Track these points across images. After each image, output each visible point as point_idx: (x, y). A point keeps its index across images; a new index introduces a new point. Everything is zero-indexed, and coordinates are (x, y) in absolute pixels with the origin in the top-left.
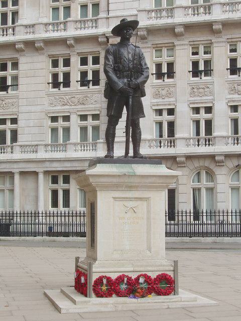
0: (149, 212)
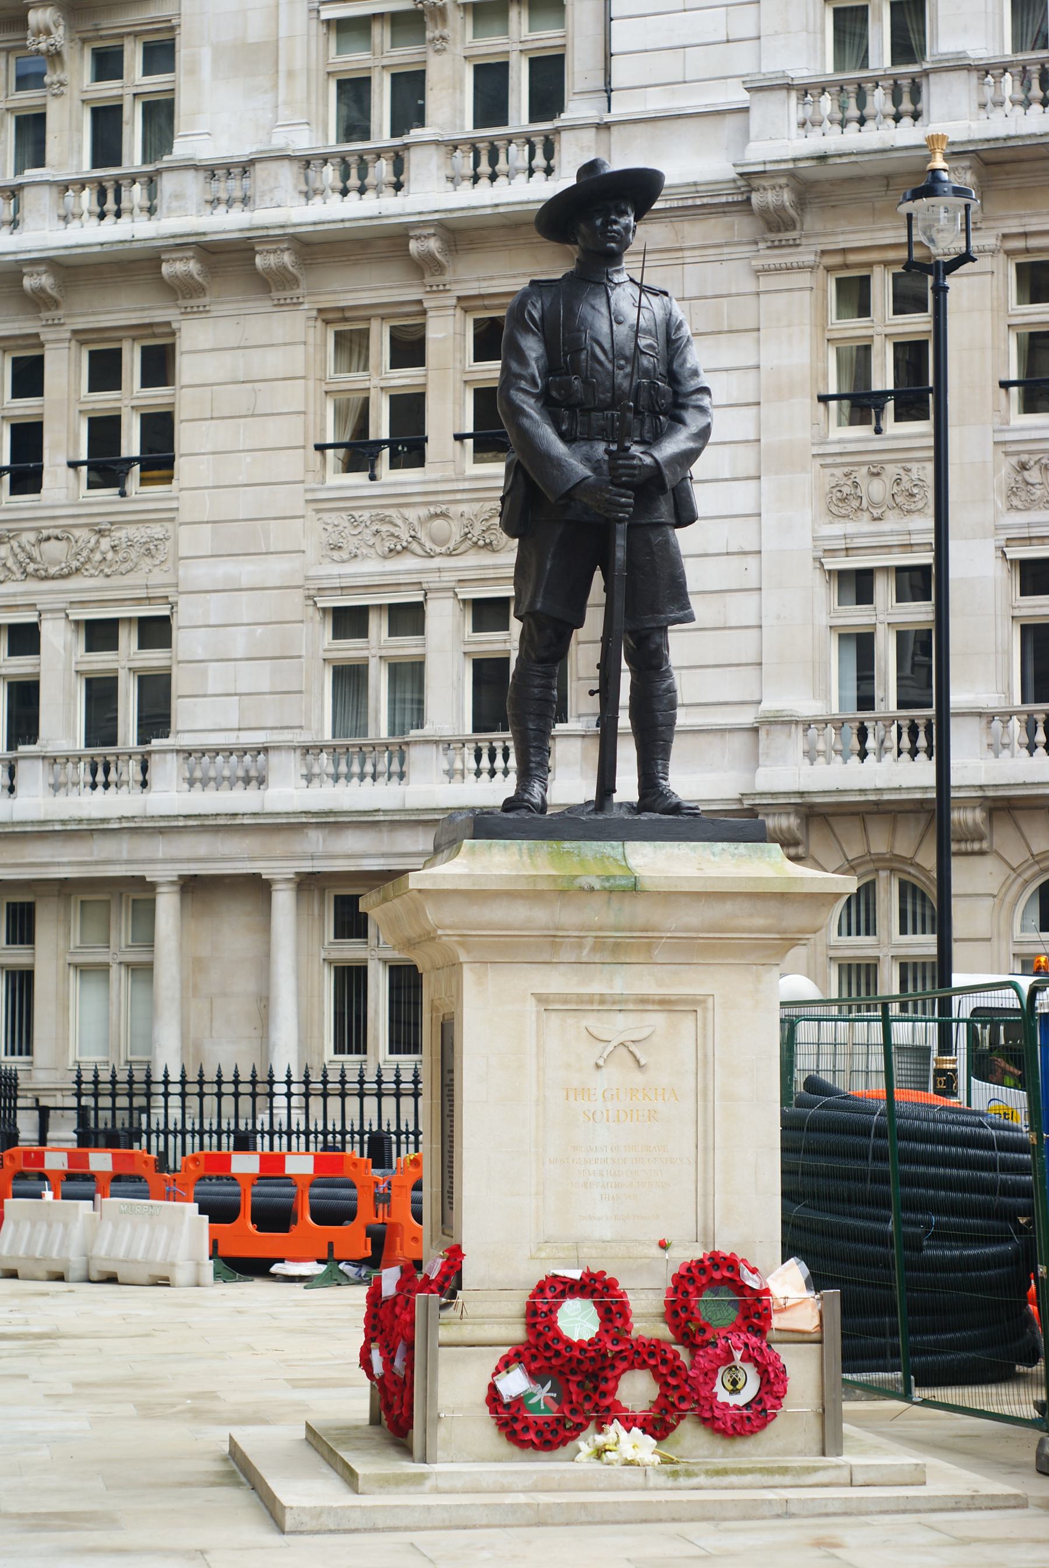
0: (703, 1062)
